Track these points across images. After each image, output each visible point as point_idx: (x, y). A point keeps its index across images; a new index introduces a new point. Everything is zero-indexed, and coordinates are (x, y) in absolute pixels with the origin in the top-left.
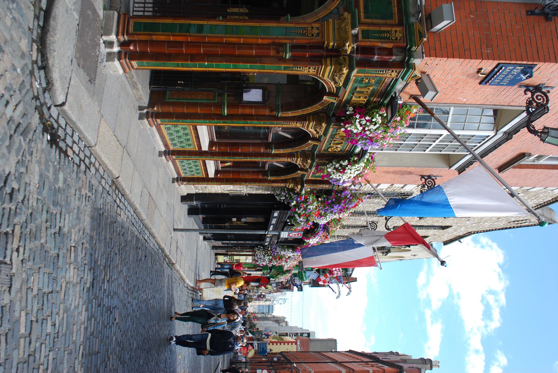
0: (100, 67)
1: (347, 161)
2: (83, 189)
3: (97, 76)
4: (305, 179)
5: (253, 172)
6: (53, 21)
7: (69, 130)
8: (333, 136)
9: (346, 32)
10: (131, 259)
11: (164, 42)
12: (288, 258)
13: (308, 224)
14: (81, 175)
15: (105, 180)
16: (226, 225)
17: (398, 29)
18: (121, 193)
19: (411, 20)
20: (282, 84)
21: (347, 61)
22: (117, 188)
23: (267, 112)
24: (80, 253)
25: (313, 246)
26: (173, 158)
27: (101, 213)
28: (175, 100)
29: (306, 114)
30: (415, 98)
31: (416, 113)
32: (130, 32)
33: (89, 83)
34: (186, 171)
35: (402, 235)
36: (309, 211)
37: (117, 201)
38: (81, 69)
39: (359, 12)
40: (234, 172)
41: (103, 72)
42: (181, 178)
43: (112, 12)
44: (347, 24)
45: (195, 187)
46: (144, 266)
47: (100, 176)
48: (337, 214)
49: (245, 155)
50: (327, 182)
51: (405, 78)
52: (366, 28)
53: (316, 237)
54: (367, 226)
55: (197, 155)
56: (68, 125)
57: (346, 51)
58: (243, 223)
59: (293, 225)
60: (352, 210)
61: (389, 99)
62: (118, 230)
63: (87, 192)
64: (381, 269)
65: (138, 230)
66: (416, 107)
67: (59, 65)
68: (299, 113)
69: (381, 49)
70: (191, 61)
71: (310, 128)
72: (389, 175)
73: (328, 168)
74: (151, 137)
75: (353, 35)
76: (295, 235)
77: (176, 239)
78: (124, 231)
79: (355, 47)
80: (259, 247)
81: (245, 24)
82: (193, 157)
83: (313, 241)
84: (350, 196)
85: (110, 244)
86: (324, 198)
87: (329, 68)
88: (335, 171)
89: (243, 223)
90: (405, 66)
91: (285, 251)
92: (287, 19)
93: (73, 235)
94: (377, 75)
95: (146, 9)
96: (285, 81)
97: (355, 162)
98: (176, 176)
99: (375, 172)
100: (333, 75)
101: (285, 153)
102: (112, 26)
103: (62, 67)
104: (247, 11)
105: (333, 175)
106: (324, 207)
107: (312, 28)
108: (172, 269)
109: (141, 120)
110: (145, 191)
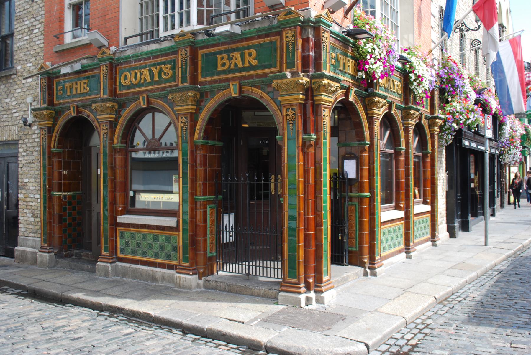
0: (329, 310)
1: (411, 75)
2: (450, 332)
3: (338, 313)
4: (429, 115)
5: (424, 167)
6: (291, 349)
7: (392, 342)
8: (387, 90)
9: (290, 83)
10: (520, 288)
11: (305, 251)
12: (512, 129)
13: (476, 110)
14: (435, 333)
15: (438, 310)
16: (478, 193)
17: (284, 35)
18: (451, 296)
19: (276, 24)
20: (339, 142)
21: (316, 80)
22: (446, 300)
23: (366, 155)
24: (518, 339)
25: (500, 103)
26: (413, 245)
27: (473, 315)
28: (357, 242)
29: (367, 117)
30: (347, 13)
31: (360, 10)
32: (297, 281)
33: (345, 320)
34: (425, 233)
35: (487, 12)
36: (463, 109)
37: (459, 300)
38: (333, 327)
39: (271, 73)
40: (425, 186)
41: (334, 307)
42: (432, 238)
43: (280, 297)
44: (283, 83)
45: (440, 224)
46: (528, 275)
47: (435, 315)
48: (465, 81)
49: (407, 175)
50: (432, 93)
51: (329, 24)
52: (285, 65)
53: (489, 101)
54: (476, 50)
55: (409, 222)
56: (386, 343)
57: (307, 82)
58: (476, 176)
59: (478, 126)
60: (460, 66)
61: (349, 38)
62: (490, 300)
63: (452, 328)
64: (523, 31)
65: (489, 281)
66: (356, 11)
67: (331, 347)
68: (365, 123)
69: (303, 50)
70: (321, 226)
71: (380, 112)
72: (422, 31)
73: (418, 93)
74: (392, 266)
75: (292, 77)
76: (489, 122)
77: (496, 244)
78: (491, 295)
79: (303, 74)
80: (500, 160)
81: (286, 177)
82: (411, 225)
83: (494, 105)
84: (445, 69)
85: (506, 308)
86: (449, 95)
87: (323, 97)
88: (421, 86)
89: (476, 176)
90: (318, 25)
91: (505, 133)
92: (280, 138)
93: (498, 344)
94: (328, 51)
95: (276, 267)
96: (336, 139)
97: (411, 67)
98: (430, 243)
99: (420, 46)
100: (330, 93)
101: (405, 136)
102: (293, 297)
103: (332, 344)
104: (273, 176)
105: (425, 87)
106: (457, 94)
107: (287, 115)
108: (529, 248)
109: (377, 274)
110: (447, 272)
